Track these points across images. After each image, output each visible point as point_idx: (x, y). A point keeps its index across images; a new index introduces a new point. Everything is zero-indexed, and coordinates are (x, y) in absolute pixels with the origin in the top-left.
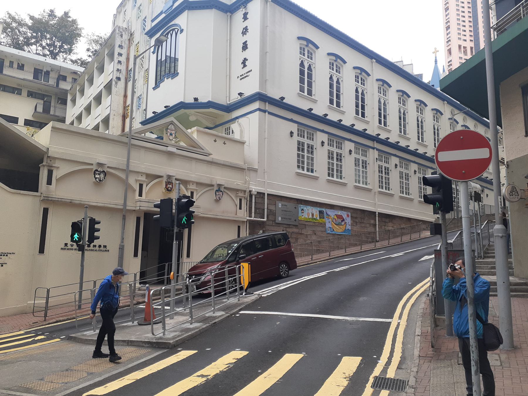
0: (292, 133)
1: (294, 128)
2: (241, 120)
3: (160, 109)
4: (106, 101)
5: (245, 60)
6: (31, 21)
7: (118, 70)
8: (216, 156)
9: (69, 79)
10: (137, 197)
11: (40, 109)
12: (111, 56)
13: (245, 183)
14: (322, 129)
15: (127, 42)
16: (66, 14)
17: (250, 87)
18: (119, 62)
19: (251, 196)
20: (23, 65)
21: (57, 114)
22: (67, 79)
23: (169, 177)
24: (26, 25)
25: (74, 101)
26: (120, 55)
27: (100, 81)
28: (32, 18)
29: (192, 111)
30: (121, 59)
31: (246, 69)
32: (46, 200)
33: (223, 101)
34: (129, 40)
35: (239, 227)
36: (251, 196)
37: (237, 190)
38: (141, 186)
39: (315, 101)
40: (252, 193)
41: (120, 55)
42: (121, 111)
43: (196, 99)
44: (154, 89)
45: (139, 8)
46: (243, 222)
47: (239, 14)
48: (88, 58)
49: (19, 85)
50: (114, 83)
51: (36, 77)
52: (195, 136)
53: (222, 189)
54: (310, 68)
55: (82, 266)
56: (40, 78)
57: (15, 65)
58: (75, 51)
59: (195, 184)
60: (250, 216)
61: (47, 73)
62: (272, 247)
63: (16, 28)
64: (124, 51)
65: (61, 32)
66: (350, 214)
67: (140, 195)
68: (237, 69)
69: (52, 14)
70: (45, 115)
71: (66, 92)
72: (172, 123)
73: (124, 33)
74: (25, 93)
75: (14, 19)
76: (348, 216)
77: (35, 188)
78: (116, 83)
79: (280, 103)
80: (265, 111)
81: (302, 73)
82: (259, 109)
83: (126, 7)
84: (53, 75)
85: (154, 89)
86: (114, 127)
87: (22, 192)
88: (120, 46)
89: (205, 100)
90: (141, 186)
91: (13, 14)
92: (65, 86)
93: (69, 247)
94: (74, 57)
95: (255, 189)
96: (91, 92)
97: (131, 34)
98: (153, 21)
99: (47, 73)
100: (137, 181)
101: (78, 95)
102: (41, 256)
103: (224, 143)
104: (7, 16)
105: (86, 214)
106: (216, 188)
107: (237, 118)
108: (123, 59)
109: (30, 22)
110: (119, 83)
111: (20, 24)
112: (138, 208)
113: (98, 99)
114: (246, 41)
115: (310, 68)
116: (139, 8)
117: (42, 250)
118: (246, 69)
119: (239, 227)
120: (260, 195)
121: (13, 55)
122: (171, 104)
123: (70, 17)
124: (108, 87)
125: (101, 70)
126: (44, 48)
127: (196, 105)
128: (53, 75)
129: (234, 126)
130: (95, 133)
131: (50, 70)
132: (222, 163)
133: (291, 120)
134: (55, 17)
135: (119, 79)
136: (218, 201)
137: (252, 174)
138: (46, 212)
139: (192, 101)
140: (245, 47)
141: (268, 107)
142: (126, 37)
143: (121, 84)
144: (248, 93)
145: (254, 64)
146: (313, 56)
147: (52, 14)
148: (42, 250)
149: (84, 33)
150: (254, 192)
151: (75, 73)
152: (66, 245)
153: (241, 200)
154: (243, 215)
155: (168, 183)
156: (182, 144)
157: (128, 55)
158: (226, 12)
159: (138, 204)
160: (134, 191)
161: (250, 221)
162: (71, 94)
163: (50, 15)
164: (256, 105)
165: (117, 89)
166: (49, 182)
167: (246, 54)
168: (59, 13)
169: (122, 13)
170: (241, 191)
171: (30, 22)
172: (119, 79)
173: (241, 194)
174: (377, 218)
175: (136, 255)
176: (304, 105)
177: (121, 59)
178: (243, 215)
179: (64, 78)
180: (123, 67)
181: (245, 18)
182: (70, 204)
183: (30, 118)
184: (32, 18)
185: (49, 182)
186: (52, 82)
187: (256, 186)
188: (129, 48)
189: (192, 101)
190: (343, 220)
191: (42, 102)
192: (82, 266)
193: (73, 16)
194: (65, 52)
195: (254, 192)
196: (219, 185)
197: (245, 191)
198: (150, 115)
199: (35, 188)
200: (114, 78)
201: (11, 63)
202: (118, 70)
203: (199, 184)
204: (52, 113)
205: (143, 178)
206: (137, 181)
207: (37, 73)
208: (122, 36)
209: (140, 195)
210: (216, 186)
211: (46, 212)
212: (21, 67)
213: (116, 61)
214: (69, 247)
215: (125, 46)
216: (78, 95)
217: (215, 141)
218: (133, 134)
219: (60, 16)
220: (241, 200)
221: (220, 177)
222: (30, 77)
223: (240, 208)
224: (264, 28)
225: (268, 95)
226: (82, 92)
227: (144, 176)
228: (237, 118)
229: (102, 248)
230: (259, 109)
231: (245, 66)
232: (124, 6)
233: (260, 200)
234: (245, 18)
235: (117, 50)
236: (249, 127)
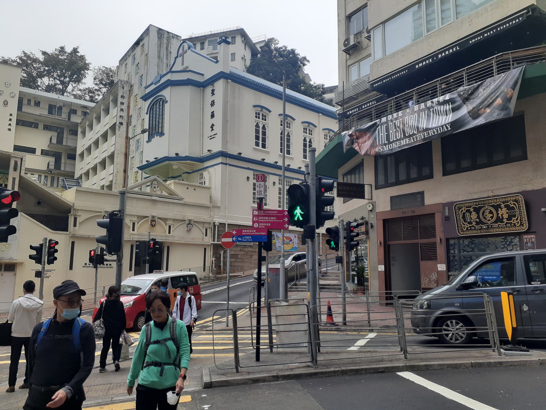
0: (248, 178)
1: (251, 174)
2: (210, 169)
3: (152, 160)
4: (111, 140)
5: (213, 125)
6: (43, 57)
7: (121, 116)
8: (187, 200)
9: (79, 113)
10: (131, 232)
11: (54, 141)
12: (115, 101)
13: (210, 217)
14: (273, 172)
15: (128, 93)
16: (75, 51)
17: (216, 146)
18: (122, 110)
19: (215, 226)
20: (39, 102)
21: (69, 144)
22: (78, 113)
23: (153, 217)
24: (40, 62)
25: (84, 133)
26: (122, 103)
27: (106, 122)
28: (44, 53)
29: (175, 162)
30: (123, 107)
31: (214, 132)
32: (73, 236)
33: (197, 154)
34: (130, 91)
35: (205, 249)
36: (215, 226)
37: (204, 223)
38: (134, 224)
39: (268, 153)
40: (216, 224)
41: (122, 103)
42: (123, 151)
43: (177, 154)
44: (147, 142)
45: (137, 65)
46: (208, 245)
47: (209, 90)
48: (95, 86)
49: (36, 120)
50: (117, 127)
51: (50, 112)
52: (172, 187)
53: (192, 223)
54: (264, 127)
55: (96, 277)
56: (54, 112)
57: (33, 103)
58: (83, 81)
59: (172, 221)
60: (214, 241)
61: (60, 108)
62: (231, 262)
63: (31, 64)
64: (125, 101)
65: (70, 65)
66: (297, 236)
67: (133, 230)
68: (208, 132)
69: (62, 50)
70: (59, 146)
71: (77, 125)
72: (155, 180)
73: (125, 85)
74: (41, 126)
75: (28, 57)
76: (295, 237)
77: (65, 229)
78: (119, 127)
79: (239, 157)
80: (226, 164)
81: (257, 131)
82: (222, 163)
83: (127, 61)
84: (65, 111)
85: (147, 142)
86: (118, 164)
87: (59, 232)
88: (122, 97)
89: (184, 155)
90: (134, 224)
91: (28, 52)
92: (76, 119)
93: (88, 265)
94: (82, 87)
95: (217, 221)
96: (100, 128)
97: (131, 86)
98: (146, 88)
99: (60, 108)
100: (131, 221)
101: (87, 129)
102: (71, 271)
103: (195, 190)
104: (23, 55)
105: (98, 245)
106: (187, 222)
107: (207, 167)
108: (125, 107)
109: (41, 58)
110: (122, 127)
111: (35, 60)
112: (131, 239)
113: (105, 136)
114: (213, 112)
115: (264, 127)
116: (137, 65)
117: (71, 268)
118: (214, 132)
119: (205, 249)
120: (222, 225)
121: (30, 94)
122: (160, 157)
123: (78, 52)
124: (113, 128)
125: (107, 111)
126: (55, 79)
127: (178, 158)
128: (65, 111)
129: (205, 174)
130: (102, 191)
131: (62, 105)
132: (192, 204)
133: (248, 169)
134: (66, 53)
135: (121, 124)
136: (189, 231)
137: (216, 210)
138: (73, 243)
139: (174, 156)
140: (213, 116)
141: (229, 161)
142: (127, 88)
143: (124, 128)
144: (215, 150)
145: (218, 129)
146: (267, 118)
147: (62, 50)
148: (71, 268)
149: (91, 67)
150: (217, 224)
151: (85, 107)
152: (86, 264)
153: (206, 230)
154: (208, 240)
155: (152, 221)
156: (164, 193)
157: (129, 103)
158: (200, 87)
159: (132, 236)
160: (129, 227)
161: (214, 244)
162: (81, 127)
163: (60, 51)
164: (219, 160)
165: (120, 132)
166: (75, 225)
167: (213, 121)
168: (69, 50)
169: (124, 65)
170: (207, 223)
171: (41, 58)
172: (121, 124)
173: (206, 226)
174: (222, 259)
175: (131, 270)
176: (258, 157)
177: (123, 107)
178: (208, 240)
179: (74, 112)
180: (124, 114)
181: (213, 93)
182: (87, 238)
183: (46, 148)
184: (44, 53)
185: (75, 225)
186: (64, 116)
187: (219, 218)
188: (130, 97)
189: (174, 156)
190: (291, 240)
191: (56, 134)
192: (96, 277)
193: (81, 52)
194: (75, 82)
195: (217, 224)
196: (190, 220)
197: (210, 223)
198: (145, 163)
199: (65, 229)
200: (118, 123)
201: (29, 101)
202: (121, 116)
203: (175, 220)
204: (64, 143)
205: (135, 219)
206: (131, 221)
207: (51, 108)
208: (123, 88)
209: (133, 230)
210: (187, 221)
211: (73, 243)
212: (37, 104)
213: (119, 103)
214: (88, 265)
215: (126, 96)
216: (87, 129)
217: (188, 188)
218: (128, 190)
219: (69, 52)
220: (206, 230)
221: (191, 214)
222: (45, 112)
223: (206, 235)
224: (225, 103)
225: (229, 153)
226: (91, 127)
227: (136, 217)
228: (207, 167)
229: (108, 266)
230: (222, 163)
231: (213, 130)
232: (126, 60)
233: (222, 229)
234: (213, 93)
235: (120, 100)
236: (214, 175)
